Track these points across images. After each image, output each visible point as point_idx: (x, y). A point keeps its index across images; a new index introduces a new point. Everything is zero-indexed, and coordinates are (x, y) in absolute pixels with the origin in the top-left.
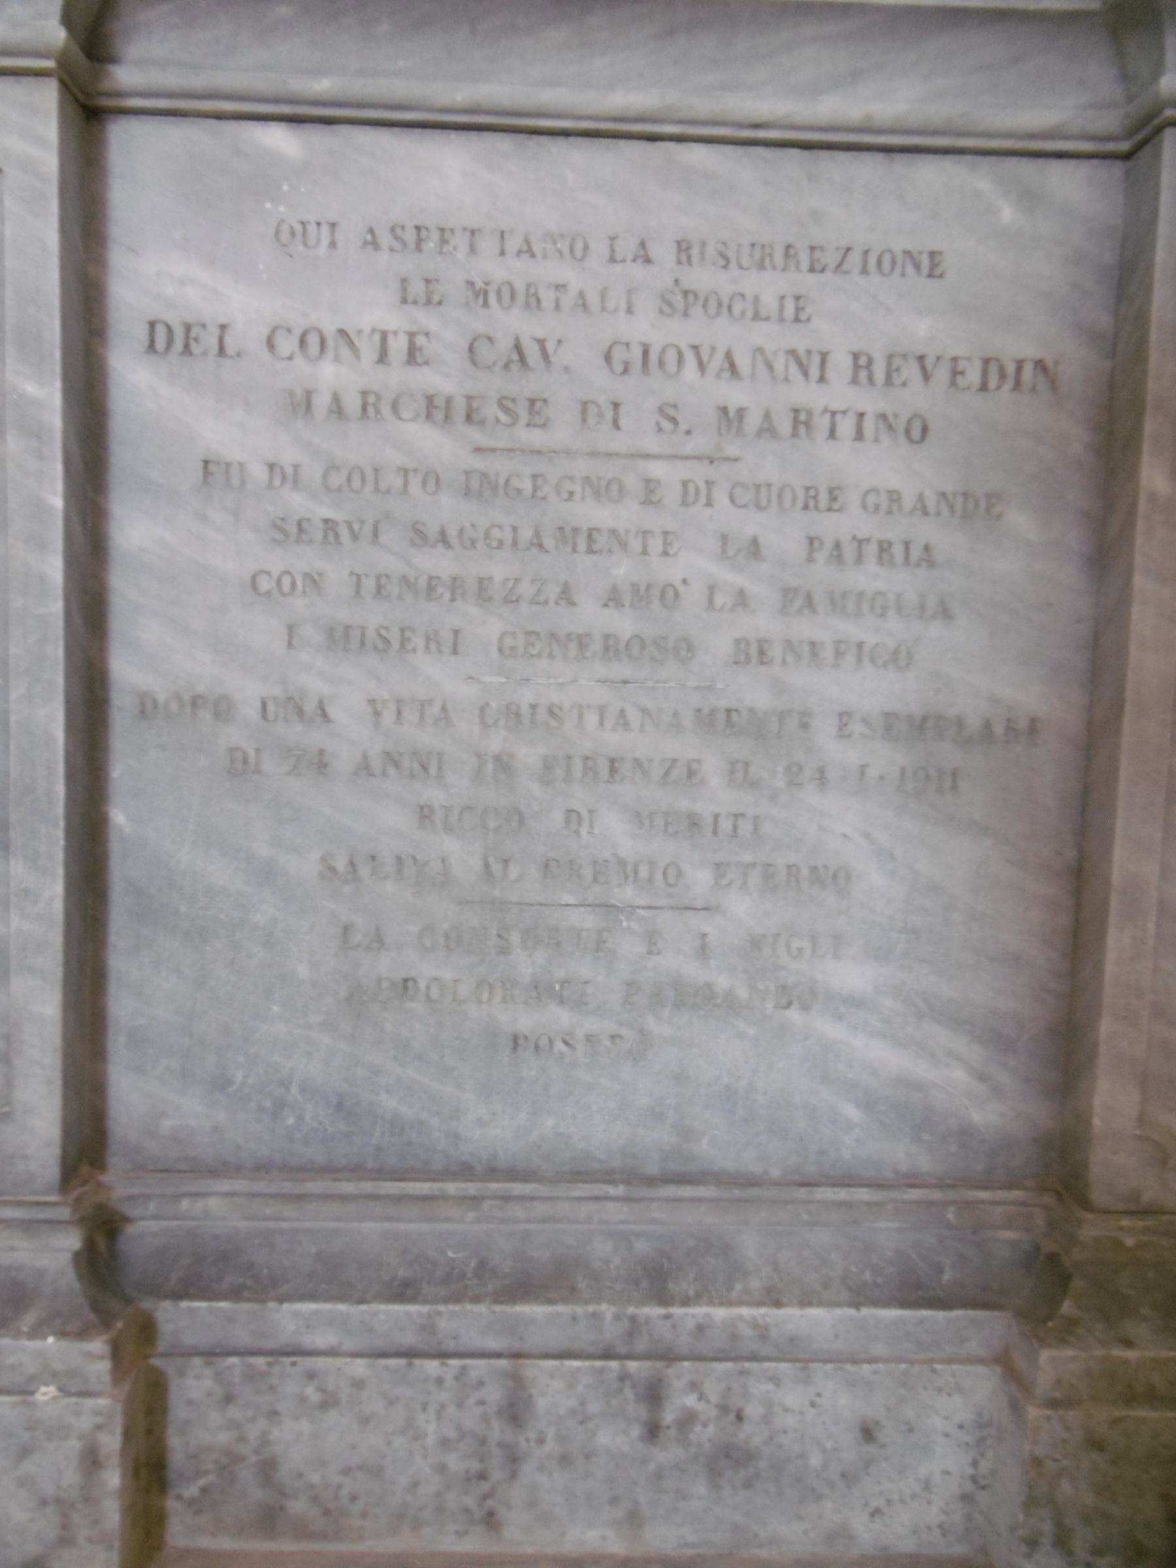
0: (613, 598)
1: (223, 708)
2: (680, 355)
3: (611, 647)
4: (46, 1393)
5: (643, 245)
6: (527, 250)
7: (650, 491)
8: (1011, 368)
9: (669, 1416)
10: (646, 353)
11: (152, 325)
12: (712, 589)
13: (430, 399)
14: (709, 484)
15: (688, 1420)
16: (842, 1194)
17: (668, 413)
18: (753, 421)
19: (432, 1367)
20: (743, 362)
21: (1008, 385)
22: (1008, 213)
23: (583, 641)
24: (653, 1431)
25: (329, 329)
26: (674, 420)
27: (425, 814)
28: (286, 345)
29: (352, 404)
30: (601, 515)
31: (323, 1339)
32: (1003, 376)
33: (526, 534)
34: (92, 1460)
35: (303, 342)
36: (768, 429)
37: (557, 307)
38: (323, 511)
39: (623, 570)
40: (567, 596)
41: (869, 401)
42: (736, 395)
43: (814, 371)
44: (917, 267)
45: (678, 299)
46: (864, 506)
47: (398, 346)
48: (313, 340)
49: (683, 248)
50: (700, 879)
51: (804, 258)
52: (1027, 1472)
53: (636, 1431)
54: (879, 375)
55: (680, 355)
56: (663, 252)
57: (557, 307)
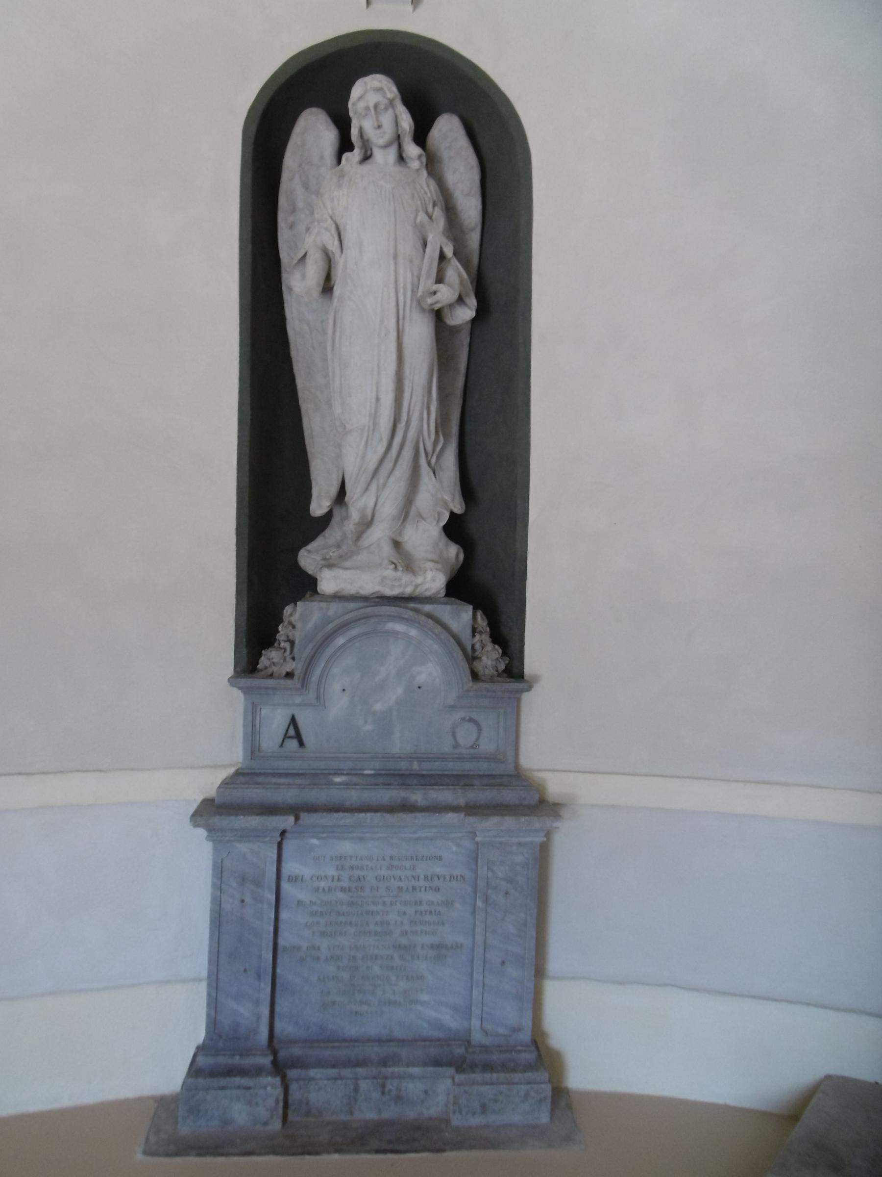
0: (377, 924)
1: (299, 949)
2: (390, 877)
3: (376, 933)
4: (269, 1088)
5: (383, 857)
6: (361, 859)
7: (384, 903)
8: (455, 877)
9: (387, 1090)
10: (384, 877)
11: (289, 877)
12: (396, 922)
13: (342, 888)
14: (396, 901)
15: (390, 1091)
16: (423, 1043)
17: (388, 889)
18: (405, 888)
19: (339, 1082)
20: (403, 878)
21: (455, 880)
22: (454, 848)
23: (370, 933)
24: (383, 1093)
25: (323, 875)
26: (389, 890)
27: (338, 968)
28: (315, 879)
29: (326, 889)
30: (373, 908)
31: (319, 1076)
32: (454, 878)
33: (360, 912)
34: (277, 1101)
35: (317, 879)
36: (407, 890)
37: (367, 869)
38: (320, 910)
39: (378, 918)
40: (367, 924)
41: (428, 884)
42: (401, 884)
43: (417, 879)
44: (437, 859)
45: (390, 867)
46: (427, 904)
47: (336, 878)
48: (320, 878)
49: (391, 858)
50: (393, 979)
51: (415, 858)
52: (308, 1114)
53: (380, 1093)
54: (429, 879)
55: (390, 877)
56: (388, 858)
57: (367, 869)
